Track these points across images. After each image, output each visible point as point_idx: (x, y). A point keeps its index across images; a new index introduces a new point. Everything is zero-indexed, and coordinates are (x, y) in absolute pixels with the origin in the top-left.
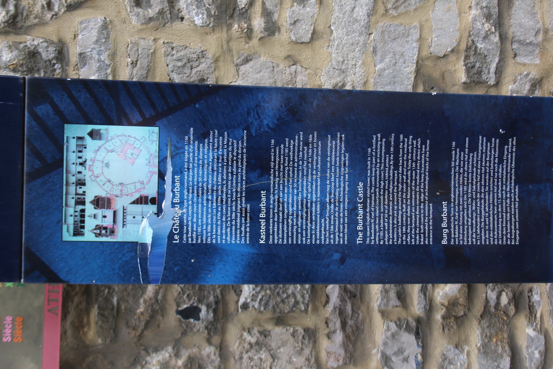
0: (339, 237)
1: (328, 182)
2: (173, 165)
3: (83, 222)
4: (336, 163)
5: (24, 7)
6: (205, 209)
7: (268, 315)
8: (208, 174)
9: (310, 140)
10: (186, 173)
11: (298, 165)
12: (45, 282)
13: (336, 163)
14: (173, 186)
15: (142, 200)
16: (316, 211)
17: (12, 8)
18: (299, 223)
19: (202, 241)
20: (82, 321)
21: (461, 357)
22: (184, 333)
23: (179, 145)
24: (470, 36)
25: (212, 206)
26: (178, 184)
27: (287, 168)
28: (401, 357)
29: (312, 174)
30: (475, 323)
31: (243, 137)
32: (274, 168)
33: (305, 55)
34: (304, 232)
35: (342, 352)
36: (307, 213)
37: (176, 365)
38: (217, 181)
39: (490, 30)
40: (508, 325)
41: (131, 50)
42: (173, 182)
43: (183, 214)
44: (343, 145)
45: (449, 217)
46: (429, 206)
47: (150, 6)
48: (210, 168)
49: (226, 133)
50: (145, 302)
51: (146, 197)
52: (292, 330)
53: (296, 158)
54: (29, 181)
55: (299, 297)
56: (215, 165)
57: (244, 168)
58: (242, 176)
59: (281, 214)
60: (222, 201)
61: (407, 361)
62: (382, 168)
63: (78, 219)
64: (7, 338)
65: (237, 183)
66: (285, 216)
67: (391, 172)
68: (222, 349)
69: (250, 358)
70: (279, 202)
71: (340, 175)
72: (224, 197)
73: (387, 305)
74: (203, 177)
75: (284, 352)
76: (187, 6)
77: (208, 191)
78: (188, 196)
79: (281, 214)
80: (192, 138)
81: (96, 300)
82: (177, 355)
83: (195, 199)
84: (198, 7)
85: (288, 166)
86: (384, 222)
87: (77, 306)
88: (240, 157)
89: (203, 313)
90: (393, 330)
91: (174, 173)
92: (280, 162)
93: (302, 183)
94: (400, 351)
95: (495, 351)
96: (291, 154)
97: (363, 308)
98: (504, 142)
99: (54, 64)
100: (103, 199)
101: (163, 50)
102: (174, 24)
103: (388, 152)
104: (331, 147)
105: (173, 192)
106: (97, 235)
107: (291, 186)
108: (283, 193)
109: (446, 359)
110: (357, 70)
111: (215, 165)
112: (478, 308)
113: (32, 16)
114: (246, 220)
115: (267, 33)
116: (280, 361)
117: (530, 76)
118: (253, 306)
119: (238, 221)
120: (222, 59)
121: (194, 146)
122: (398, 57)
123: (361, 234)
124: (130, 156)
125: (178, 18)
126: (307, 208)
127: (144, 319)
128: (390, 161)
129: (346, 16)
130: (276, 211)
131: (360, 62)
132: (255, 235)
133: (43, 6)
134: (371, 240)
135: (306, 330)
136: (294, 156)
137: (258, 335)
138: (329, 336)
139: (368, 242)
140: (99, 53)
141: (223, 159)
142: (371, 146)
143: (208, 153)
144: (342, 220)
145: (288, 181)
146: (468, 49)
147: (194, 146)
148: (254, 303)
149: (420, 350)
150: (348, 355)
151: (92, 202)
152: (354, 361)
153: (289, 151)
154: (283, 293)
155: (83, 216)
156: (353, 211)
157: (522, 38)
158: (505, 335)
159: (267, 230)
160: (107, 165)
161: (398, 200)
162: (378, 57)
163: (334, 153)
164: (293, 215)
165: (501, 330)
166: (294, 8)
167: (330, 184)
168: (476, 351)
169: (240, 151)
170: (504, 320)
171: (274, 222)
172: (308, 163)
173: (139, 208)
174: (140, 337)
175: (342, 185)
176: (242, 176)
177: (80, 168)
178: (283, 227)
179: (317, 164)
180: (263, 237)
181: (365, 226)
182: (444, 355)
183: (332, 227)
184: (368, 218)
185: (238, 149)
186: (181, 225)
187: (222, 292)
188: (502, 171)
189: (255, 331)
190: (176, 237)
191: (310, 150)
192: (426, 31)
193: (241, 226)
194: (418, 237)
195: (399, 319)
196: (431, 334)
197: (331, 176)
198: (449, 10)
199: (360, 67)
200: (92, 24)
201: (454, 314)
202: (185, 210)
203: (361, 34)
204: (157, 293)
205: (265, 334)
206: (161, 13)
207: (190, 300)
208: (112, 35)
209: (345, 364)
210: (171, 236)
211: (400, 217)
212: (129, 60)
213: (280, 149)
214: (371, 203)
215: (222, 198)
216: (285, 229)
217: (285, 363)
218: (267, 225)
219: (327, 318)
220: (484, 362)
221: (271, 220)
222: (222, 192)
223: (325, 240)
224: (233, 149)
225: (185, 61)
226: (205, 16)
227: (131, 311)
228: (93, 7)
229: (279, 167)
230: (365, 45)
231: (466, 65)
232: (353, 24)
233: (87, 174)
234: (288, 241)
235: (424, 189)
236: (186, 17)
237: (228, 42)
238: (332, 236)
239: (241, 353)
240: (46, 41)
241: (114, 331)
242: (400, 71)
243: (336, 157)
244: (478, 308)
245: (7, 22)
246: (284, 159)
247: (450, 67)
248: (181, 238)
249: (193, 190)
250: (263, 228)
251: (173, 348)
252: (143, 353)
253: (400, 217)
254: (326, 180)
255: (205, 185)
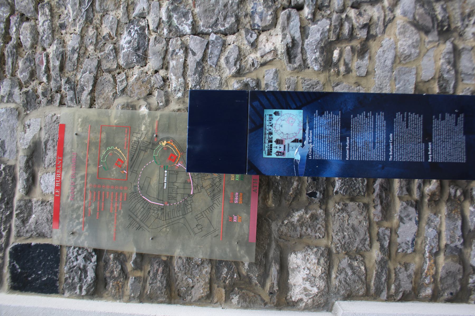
0: (381, 158)
1: (376, 133)
2: (309, 126)
3: (271, 150)
4: (380, 125)
5: (243, 66)
6: (322, 145)
7: (347, 197)
8: (324, 130)
9: (368, 115)
10: (314, 129)
11: (363, 126)
12: (255, 175)
13: (380, 125)
14: (309, 135)
15: (296, 141)
16: (371, 146)
17: (238, 66)
18: (364, 151)
19: (321, 158)
20: (266, 197)
21: (437, 219)
22: (310, 204)
23: (311, 118)
24: (440, 72)
25: (326, 143)
26: (311, 134)
27: (358, 127)
28: (408, 218)
29: (369, 130)
30: (444, 204)
31: (339, 114)
32: (353, 127)
33: (363, 82)
34: (366, 155)
35: (381, 215)
36: (367, 147)
37: (306, 217)
38: (328, 133)
39: (449, 69)
40: (460, 205)
41: (287, 81)
42: (309, 133)
43: (313, 147)
44: (383, 118)
45: (432, 149)
46: (422, 145)
47: (295, 63)
48: (325, 127)
49: (331, 112)
50: (293, 189)
51: (298, 140)
52: (357, 204)
53: (362, 123)
54: (250, 133)
55: (361, 189)
56: (327, 126)
57: (339, 127)
58: (338, 131)
59: (355, 147)
60: (330, 141)
61: (411, 220)
62: (401, 127)
63: (269, 148)
64: (236, 202)
65: (336, 134)
66: (357, 148)
67: (405, 129)
68: (326, 212)
69: (338, 216)
70: (355, 142)
71: (382, 131)
72: (331, 140)
73: (402, 194)
74: (322, 131)
75: (354, 214)
76: (311, 62)
77: (324, 137)
78: (315, 139)
79: (355, 147)
80: (317, 114)
81: (272, 188)
82: (306, 213)
83: (318, 141)
84: (316, 62)
85: (359, 126)
86: (402, 151)
87: (264, 190)
88: (337, 122)
89: (318, 195)
90: (404, 206)
91: (309, 129)
92: (355, 124)
93: (365, 134)
94: (408, 216)
95: (454, 217)
96: (360, 121)
97: (391, 195)
98: (458, 116)
99: (255, 89)
100: (280, 140)
101: (301, 81)
102: (305, 70)
103: (403, 120)
104: (378, 118)
105: (309, 138)
106: (277, 155)
107: (360, 135)
108: (357, 138)
109: (429, 220)
110: (387, 88)
111: (327, 126)
112: (446, 197)
113: (246, 69)
114: (340, 150)
115: (346, 73)
116: (352, 218)
117: (470, 90)
118: (340, 193)
119: (337, 150)
120: (326, 84)
121: (318, 118)
122: (406, 82)
123: (391, 156)
124: (291, 122)
125: (307, 67)
126: (367, 145)
127: (292, 196)
128: (404, 124)
129: (382, 64)
130: (353, 146)
131: (389, 84)
132: (344, 156)
133: (251, 65)
134: (396, 159)
135: (364, 204)
136: (361, 122)
137: (343, 206)
138: (375, 207)
139: (394, 160)
140: (274, 83)
141: (330, 124)
142: (396, 118)
143: (324, 121)
144: (382, 150)
145: (359, 133)
146: (439, 77)
147: (318, 118)
148: (341, 191)
149: (417, 215)
150: (383, 216)
151: (275, 142)
152: (386, 219)
153: (359, 120)
154: (354, 187)
155: (271, 147)
156: (388, 146)
157: (466, 72)
158: (459, 210)
159: (350, 154)
160: (281, 126)
161: (408, 142)
162: (397, 82)
163: (379, 121)
164: (361, 147)
165: (457, 207)
166: (358, 62)
167: (377, 134)
168: (444, 217)
169: (337, 120)
170: (458, 203)
171: (352, 150)
172: (367, 125)
173: (294, 144)
174: (291, 204)
175: (383, 135)
176: (338, 131)
177: (270, 127)
178: (356, 153)
179: (371, 125)
180: (348, 157)
181: (393, 153)
182: (429, 218)
183: (378, 153)
184: (395, 149)
185: (337, 119)
186: (312, 151)
187: (326, 186)
188: (457, 129)
189: (341, 203)
190: (310, 156)
191: (368, 120)
192: (419, 70)
193: (338, 152)
194: (417, 158)
195: (407, 201)
196: (423, 208)
197: (378, 131)
198: (430, 60)
199: (389, 86)
200: (270, 72)
201: (434, 199)
202: (314, 145)
203: (389, 72)
204: (298, 185)
205: (345, 205)
206: (300, 65)
207: (312, 189)
208: (279, 76)
209: (382, 220)
210: (308, 156)
211: (409, 149)
212: (286, 86)
213: (355, 119)
214: (396, 143)
215: (330, 140)
216: (357, 153)
217: (354, 218)
218: (350, 152)
219: (374, 199)
220: (448, 222)
221: (351, 150)
222: (330, 137)
223: (375, 159)
224: (335, 119)
225: (310, 85)
226: (319, 66)
227: (287, 193)
228: (271, 65)
229: (355, 127)
230: (391, 77)
231: (439, 85)
232: (385, 68)
233: (273, 130)
234: (358, 159)
235: (420, 137)
236: (311, 67)
237: (329, 77)
238: (378, 157)
239: (335, 213)
240: (252, 79)
241: (279, 202)
242: (407, 88)
243: (380, 123)
244: (446, 197)
245: (236, 72)
246: (357, 124)
247: (431, 86)
248: (312, 157)
249: (317, 136)
250: (348, 153)
251: (305, 210)
252: (292, 211)
253: (409, 149)
254: (375, 133)
255: (322, 134)
